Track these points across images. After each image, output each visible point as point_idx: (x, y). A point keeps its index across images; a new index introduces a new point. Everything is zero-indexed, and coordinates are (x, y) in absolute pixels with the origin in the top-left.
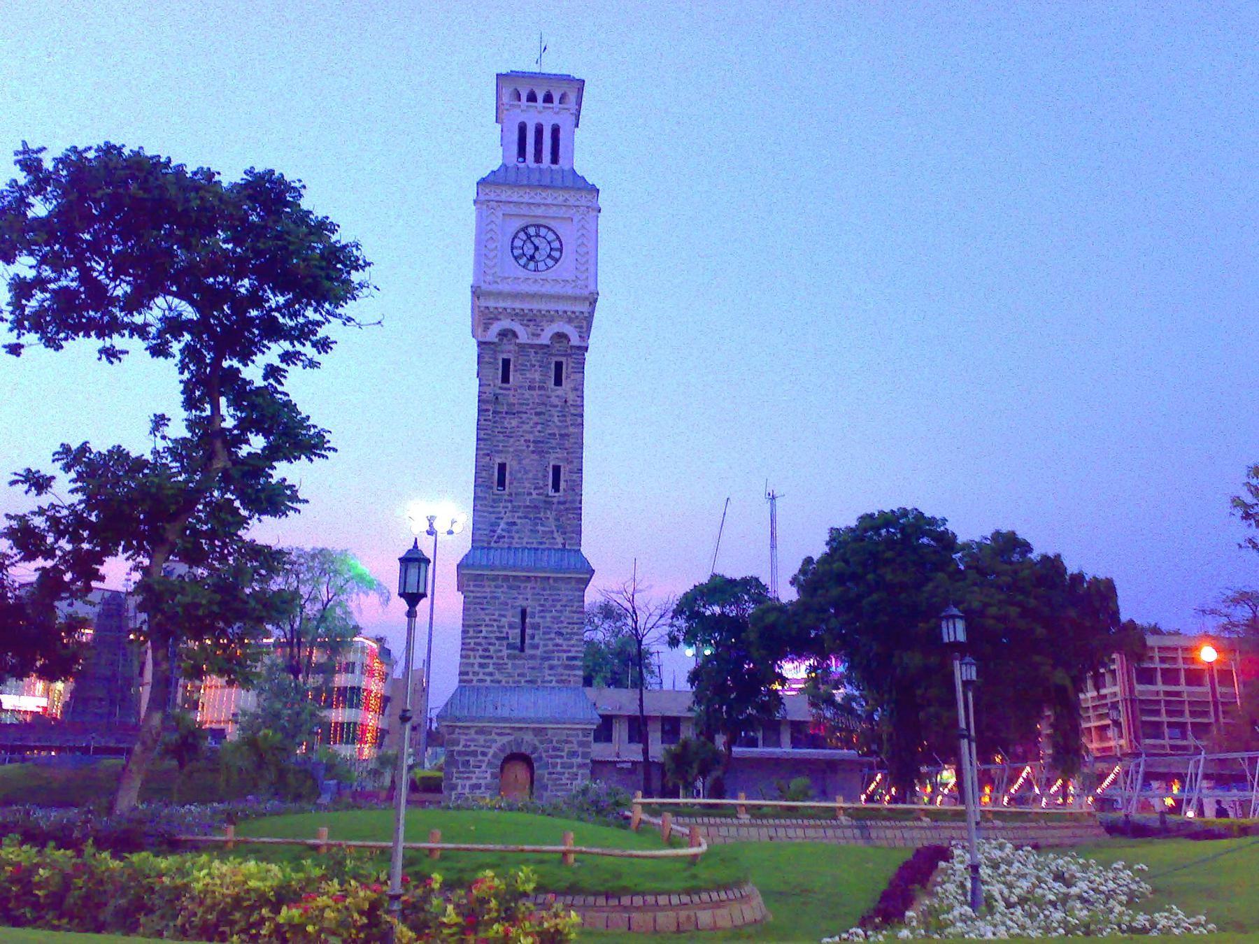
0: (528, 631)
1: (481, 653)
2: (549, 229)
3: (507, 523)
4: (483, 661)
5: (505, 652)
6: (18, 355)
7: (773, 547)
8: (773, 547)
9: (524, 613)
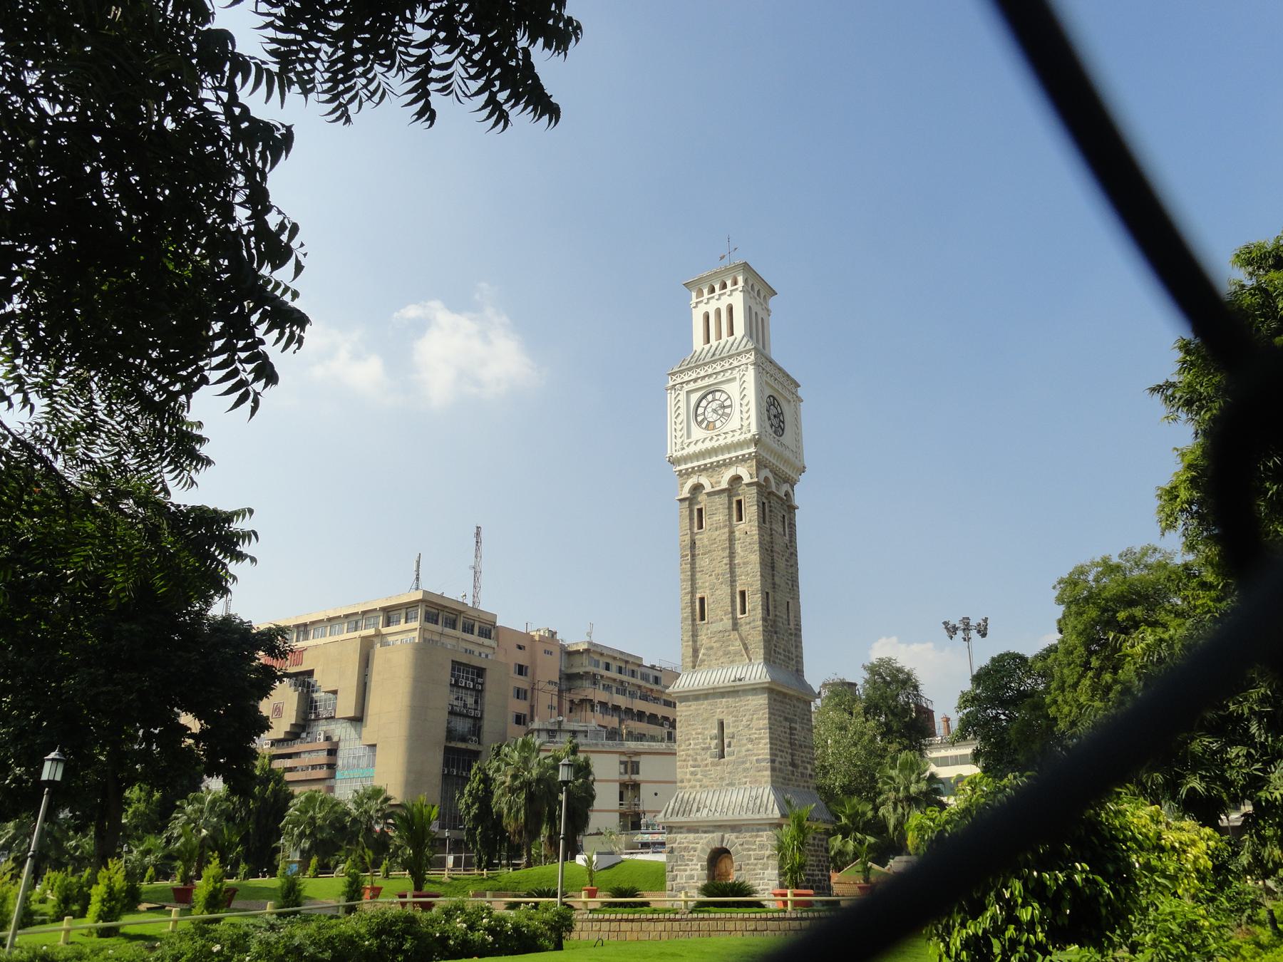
0: (726, 741)
6: (483, 670)
9: (721, 724)
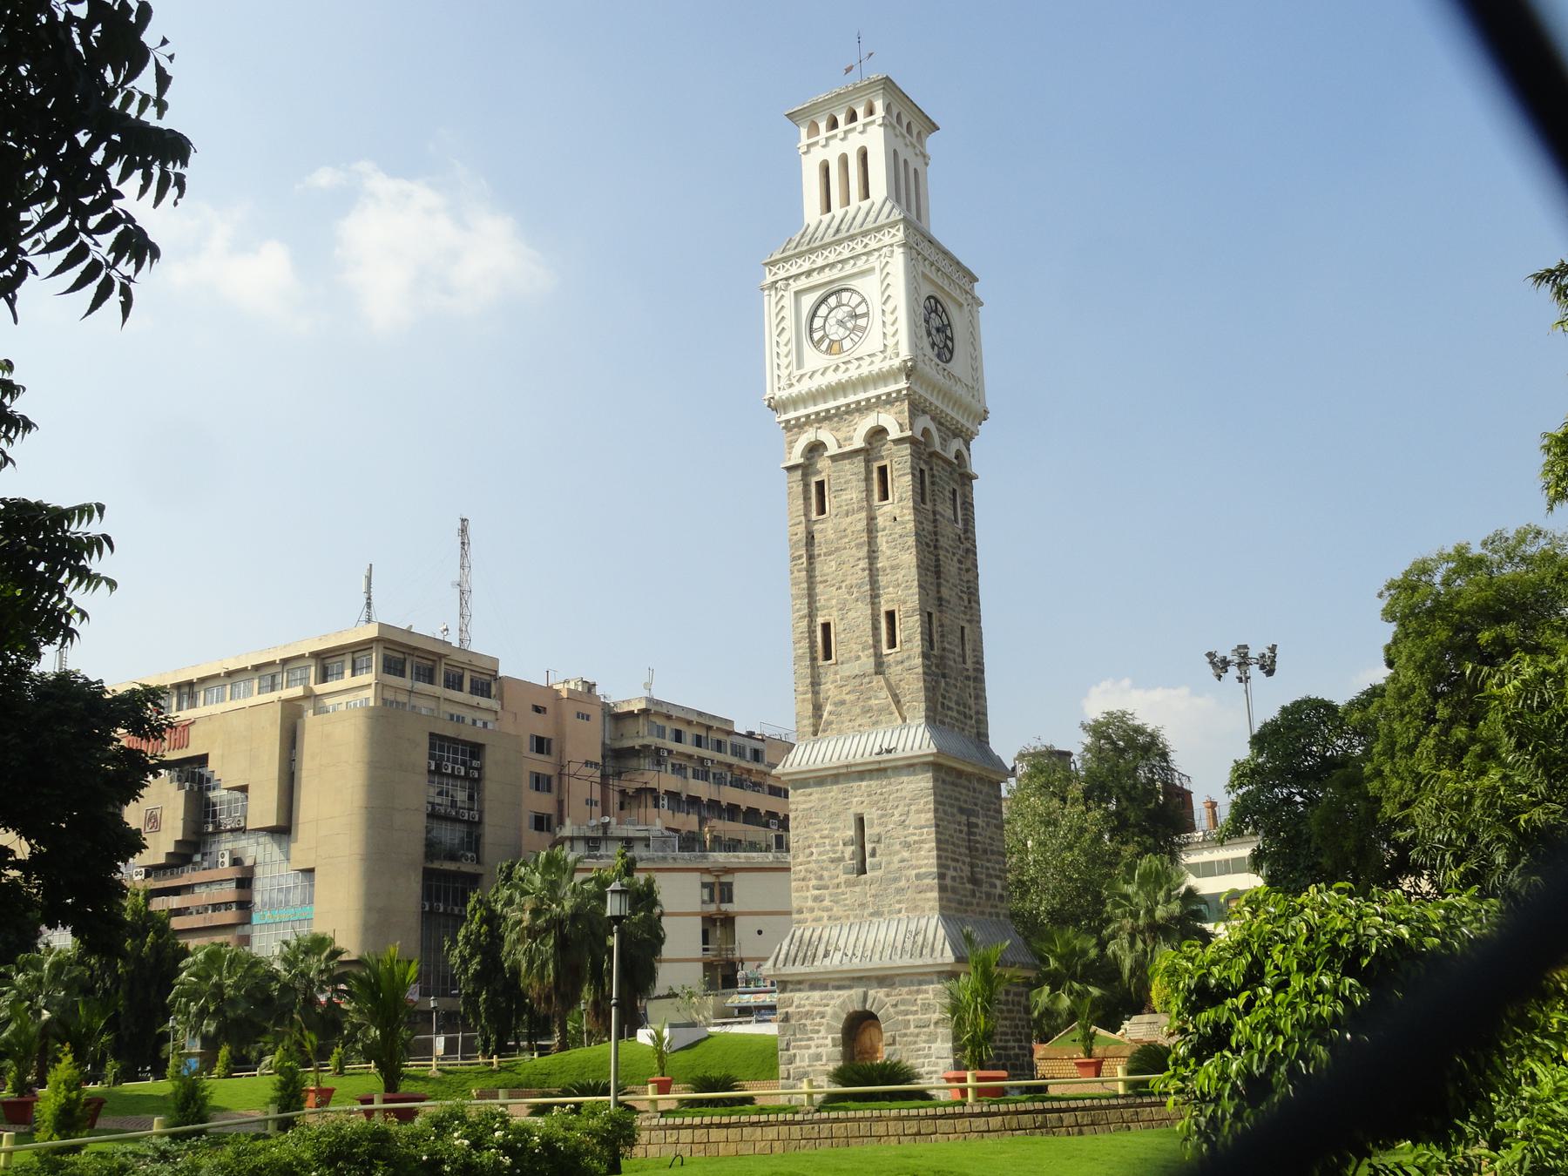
0: (868, 847)
1: (814, 882)
2: (814, 315)
3: (835, 704)
4: (817, 892)
5: (843, 878)
7: (369, 605)
8: (369, 605)
9: (860, 821)
